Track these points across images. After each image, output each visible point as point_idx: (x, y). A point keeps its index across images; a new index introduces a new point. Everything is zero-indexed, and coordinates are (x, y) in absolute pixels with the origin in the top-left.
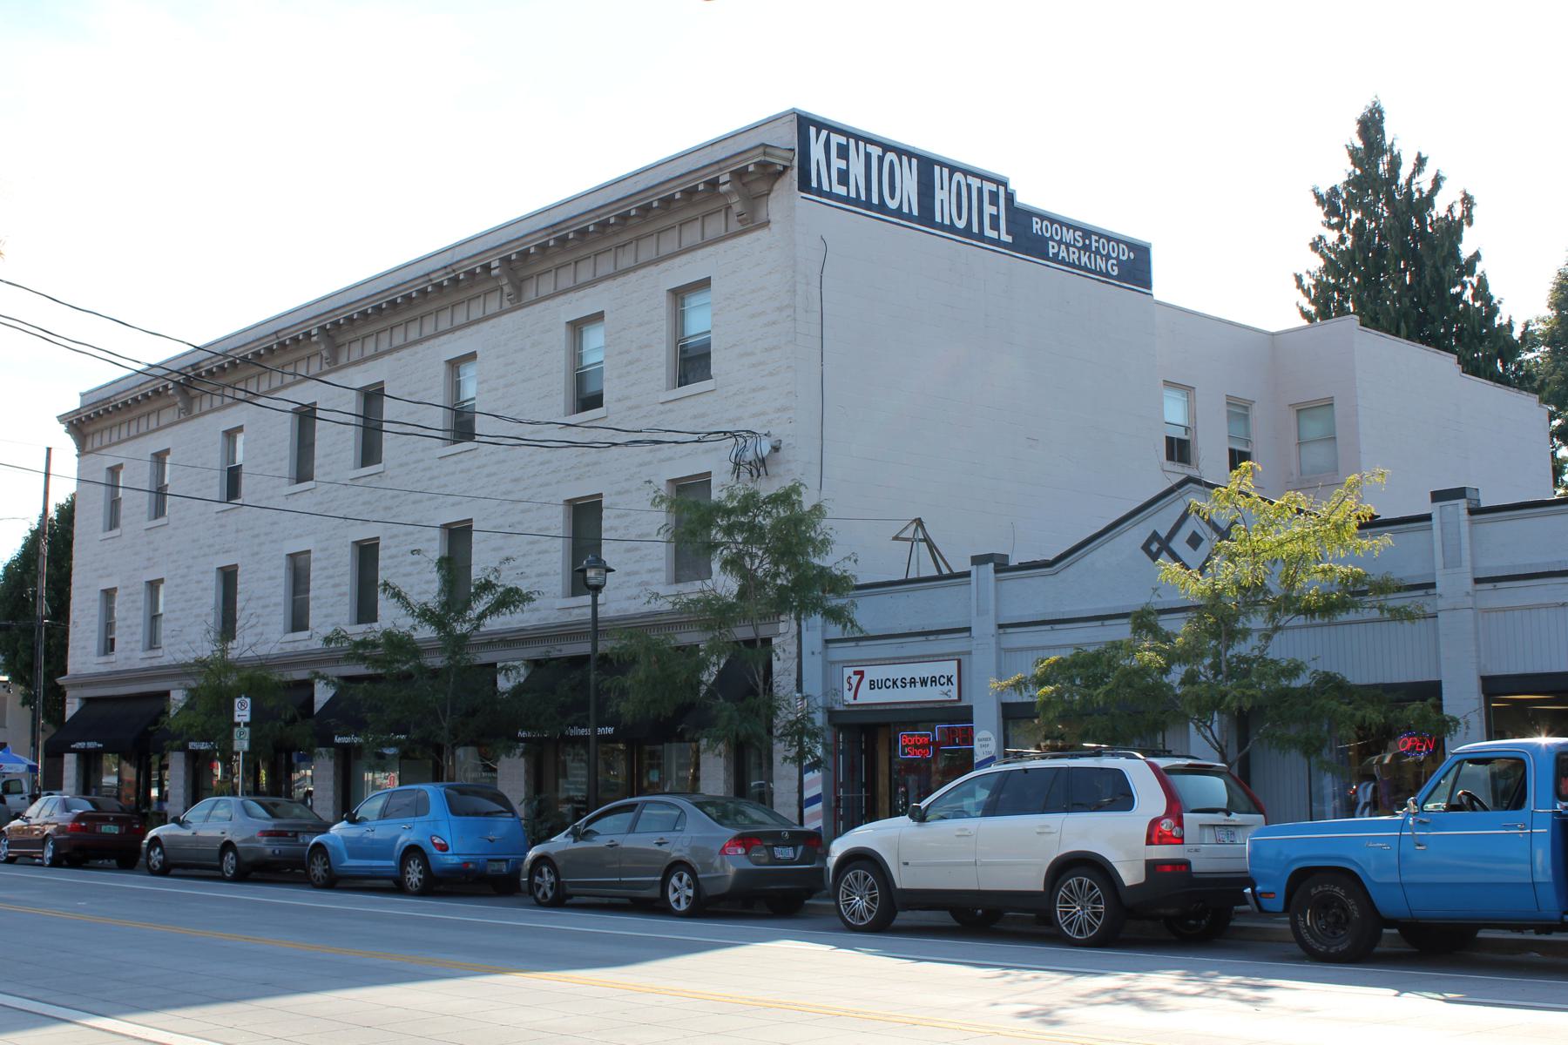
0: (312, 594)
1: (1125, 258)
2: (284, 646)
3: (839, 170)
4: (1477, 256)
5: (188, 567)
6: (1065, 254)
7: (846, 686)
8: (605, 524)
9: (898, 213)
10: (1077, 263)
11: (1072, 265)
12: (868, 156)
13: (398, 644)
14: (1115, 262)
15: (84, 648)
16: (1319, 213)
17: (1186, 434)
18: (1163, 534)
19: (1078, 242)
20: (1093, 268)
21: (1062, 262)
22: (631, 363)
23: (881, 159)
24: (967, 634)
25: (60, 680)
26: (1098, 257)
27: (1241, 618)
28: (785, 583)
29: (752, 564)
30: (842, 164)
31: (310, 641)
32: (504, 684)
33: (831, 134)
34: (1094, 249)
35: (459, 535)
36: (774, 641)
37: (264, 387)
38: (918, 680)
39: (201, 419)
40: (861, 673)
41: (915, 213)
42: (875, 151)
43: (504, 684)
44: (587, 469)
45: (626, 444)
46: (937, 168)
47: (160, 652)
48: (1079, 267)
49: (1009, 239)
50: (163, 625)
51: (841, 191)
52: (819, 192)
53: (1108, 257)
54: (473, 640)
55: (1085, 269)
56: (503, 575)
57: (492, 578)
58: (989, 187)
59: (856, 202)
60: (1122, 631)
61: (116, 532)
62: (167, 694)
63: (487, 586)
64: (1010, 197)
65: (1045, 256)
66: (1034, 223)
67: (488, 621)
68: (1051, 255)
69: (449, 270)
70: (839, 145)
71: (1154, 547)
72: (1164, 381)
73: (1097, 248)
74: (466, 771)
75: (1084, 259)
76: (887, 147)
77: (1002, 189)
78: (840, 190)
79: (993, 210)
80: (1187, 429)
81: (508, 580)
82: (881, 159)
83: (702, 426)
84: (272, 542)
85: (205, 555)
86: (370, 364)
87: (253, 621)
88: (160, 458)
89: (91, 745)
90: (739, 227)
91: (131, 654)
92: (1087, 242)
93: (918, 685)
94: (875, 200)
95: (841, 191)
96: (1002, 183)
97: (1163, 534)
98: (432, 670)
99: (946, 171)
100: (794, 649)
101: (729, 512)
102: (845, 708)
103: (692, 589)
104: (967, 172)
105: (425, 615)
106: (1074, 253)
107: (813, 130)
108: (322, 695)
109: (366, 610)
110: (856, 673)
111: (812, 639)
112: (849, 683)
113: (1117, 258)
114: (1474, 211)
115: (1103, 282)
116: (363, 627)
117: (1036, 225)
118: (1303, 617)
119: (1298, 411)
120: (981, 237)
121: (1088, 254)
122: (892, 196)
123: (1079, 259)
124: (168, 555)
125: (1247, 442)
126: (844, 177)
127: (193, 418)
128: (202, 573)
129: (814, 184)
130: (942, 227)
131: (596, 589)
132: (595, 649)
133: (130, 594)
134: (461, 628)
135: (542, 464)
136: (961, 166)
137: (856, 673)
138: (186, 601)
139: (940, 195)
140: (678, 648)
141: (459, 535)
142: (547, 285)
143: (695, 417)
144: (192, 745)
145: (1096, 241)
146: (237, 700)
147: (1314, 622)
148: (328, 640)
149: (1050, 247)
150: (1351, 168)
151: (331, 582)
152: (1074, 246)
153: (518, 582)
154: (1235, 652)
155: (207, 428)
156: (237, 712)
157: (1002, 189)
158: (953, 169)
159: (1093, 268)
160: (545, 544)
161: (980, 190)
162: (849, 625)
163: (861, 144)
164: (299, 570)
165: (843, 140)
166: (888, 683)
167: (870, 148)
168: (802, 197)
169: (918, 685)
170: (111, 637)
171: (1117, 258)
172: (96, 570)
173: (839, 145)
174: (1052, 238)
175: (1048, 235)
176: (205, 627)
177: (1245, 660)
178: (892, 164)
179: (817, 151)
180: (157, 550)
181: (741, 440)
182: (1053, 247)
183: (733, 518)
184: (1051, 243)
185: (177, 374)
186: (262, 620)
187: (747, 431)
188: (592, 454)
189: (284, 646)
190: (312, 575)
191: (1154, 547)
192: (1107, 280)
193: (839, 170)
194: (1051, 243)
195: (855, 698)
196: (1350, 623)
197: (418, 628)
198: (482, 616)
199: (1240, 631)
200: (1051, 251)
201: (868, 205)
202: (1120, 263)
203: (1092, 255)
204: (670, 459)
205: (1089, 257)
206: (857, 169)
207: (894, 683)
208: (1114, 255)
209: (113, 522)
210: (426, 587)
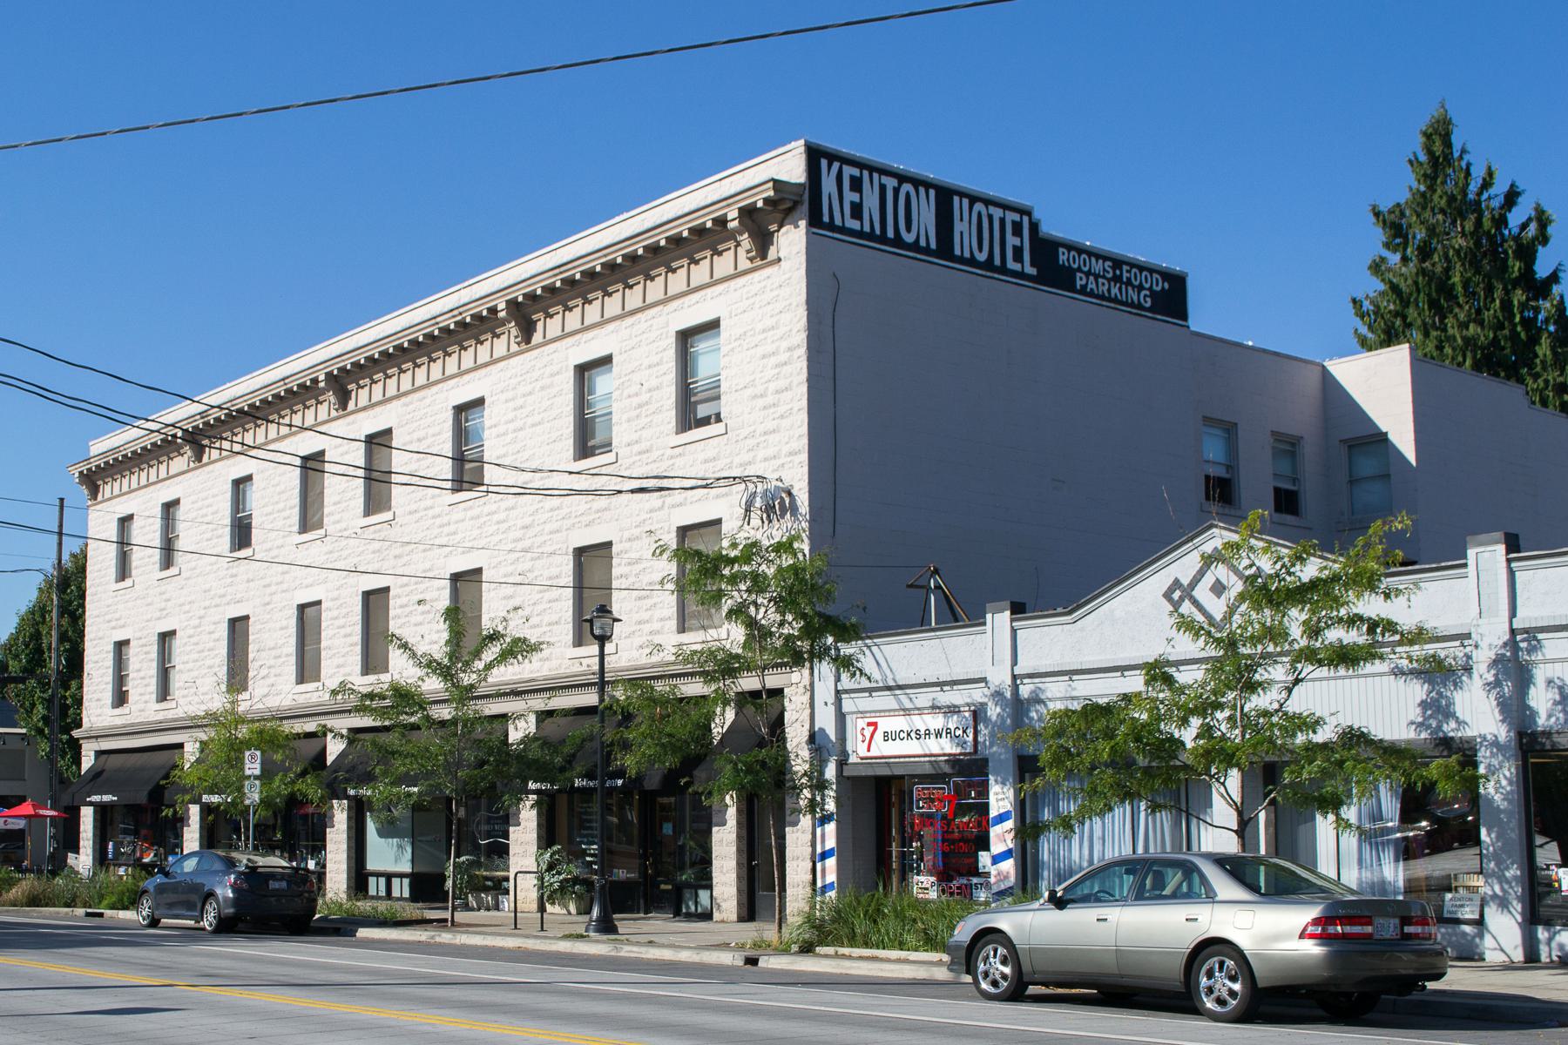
0: (323, 644)
1: (1159, 288)
2: (296, 697)
3: (852, 203)
4: (1554, 278)
5: (200, 618)
6: (1094, 286)
7: (860, 738)
8: (615, 572)
9: (915, 247)
10: (1107, 295)
11: (1102, 297)
12: (883, 188)
13: (404, 697)
14: (1148, 293)
15: (98, 700)
16: (1379, 235)
17: (1228, 472)
18: (1185, 581)
19: (1108, 272)
20: (1124, 299)
21: (1091, 294)
22: (640, 406)
23: (896, 191)
24: (983, 685)
25: (76, 733)
26: (1130, 288)
27: (1259, 669)
28: (791, 632)
29: (757, 613)
30: (855, 197)
31: (313, 694)
32: (515, 736)
33: (844, 166)
34: (1125, 279)
35: (465, 582)
36: (786, 691)
37: (260, 439)
38: (932, 731)
39: (210, 467)
40: (875, 724)
41: (933, 246)
42: (891, 183)
43: (515, 736)
44: (597, 516)
45: (632, 491)
46: (956, 199)
47: (173, 704)
48: (1110, 299)
49: (1032, 271)
50: (177, 677)
51: (855, 225)
52: (831, 226)
53: (1140, 288)
54: (481, 691)
55: (1115, 300)
56: (512, 624)
57: (500, 628)
58: (1012, 217)
59: (871, 236)
60: (1135, 683)
61: (128, 582)
62: (180, 746)
63: (494, 637)
64: (1034, 227)
65: (1072, 288)
66: (1060, 253)
67: (495, 671)
68: (1078, 287)
69: (455, 312)
70: (852, 178)
71: (1177, 595)
72: (1204, 417)
73: (1129, 279)
74: (479, 823)
75: (1115, 291)
76: (902, 178)
77: (1026, 219)
78: (854, 225)
79: (1017, 241)
80: (1228, 468)
81: (516, 629)
82: (896, 191)
83: (711, 471)
84: (283, 591)
85: (216, 606)
86: (378, 409)
87: (264, 672)
88: (170, 507)
89: (107, 798)
90: (748, 265)
91: (143, 706)
92: (1118, 272)
93: (933, 737)
94: (890, 234)
95: (855, 225)
96: (1025, 212)
97: (1185, 581)
98: (440, 722)
99: (966, 202)
100: (805, 699)
101: (731, 561)
102: (859, 761)
103: (695, 640)
104: (988, 202)
105: (432, 665)
106: (1103, 284)
107: (824, 163)
108: (334, 748)
109: (372, 661)
110: (869, 724)
111: (825, 691)
112: (863, 735)
113: (1150, 289)
114: (1550, 230)
115: (1135, 314)
116: (372, 678)
117: (1063, 256)
118: (1326, 668)
119: (1350, 447)
120: (1003, 269)
121: (1118, 285)
122: (909, 229)
123: (1109, 290)
124: (180, 605)
125: (1295, 481)
126: (857, 210)
127: (202, 466)
128: (215, 623)
129: (826, 219)
130: (961, 260)
131: (603, 640)
132: (602, 700)
133: (143, 646)
134: (467, 679)
135: (552, 510)
136: (982, 196)
137: (869, 724)
138: (199, 652)
139: (959, 227)
140: (681, 700)
141: (465, 582)
142: (554, 326)
143: (706, 461)
144: (205, 798)
145: (1127, 271)
146: (247, 753)
147: (1338, 674)
148: (334, 693)
149: (1078, 278)
150: (1415, 184)
151: (343, 631)
152: (1104, 277)
153: (526, 631)
154: (1253, 706)
155: (221, 471)
156: (248, 765)
157: (1026, 219)
158: (973, 199)
159: (1124, 299)
160: (555, 593)
161: (1002, 221)
162: (858, 673)
163: (875, 176)
164: (307, 617)
165: (856, 172)
166: (902, 735)
167: (886, 180)
168: (814, 233)
169: (933, 737)
170: (124, 689)
171: (1150, 289)
172: (109, 621)
173: (852, 178)
174: (1079, 269)
175: (1076, 266)
176: (215, 678)
177: (1266, 714)
178: (908, 195)
179: (828, 185)
180: (169, 600)
181: (751, 486)
182: (1081, 279)
183: (736, 567)
184: (1079, 275)
185: (217, 410)
186: (273, 671)
187: (758, 477)
188: (602, 502)
189: (296, 697)
190: (324, 625)
191: (1177, 595)
192: (1139, 312)
193: (852, 203)
194: (1079, 275)
195: (869, 750)
196: (1374, 675)
197: (426, 678)
198: (489, 667)
199: (1260, 684)
200: (1079, 283)
201: (883, 239)
202: (1153, 294)
203: (1124, 286)
204: (681, 505)
205: (1120, 289)
206: (871, 202)
207: (909, 735)
208: (1147, 286)
209: (123, 571)
210: (433, 638)
